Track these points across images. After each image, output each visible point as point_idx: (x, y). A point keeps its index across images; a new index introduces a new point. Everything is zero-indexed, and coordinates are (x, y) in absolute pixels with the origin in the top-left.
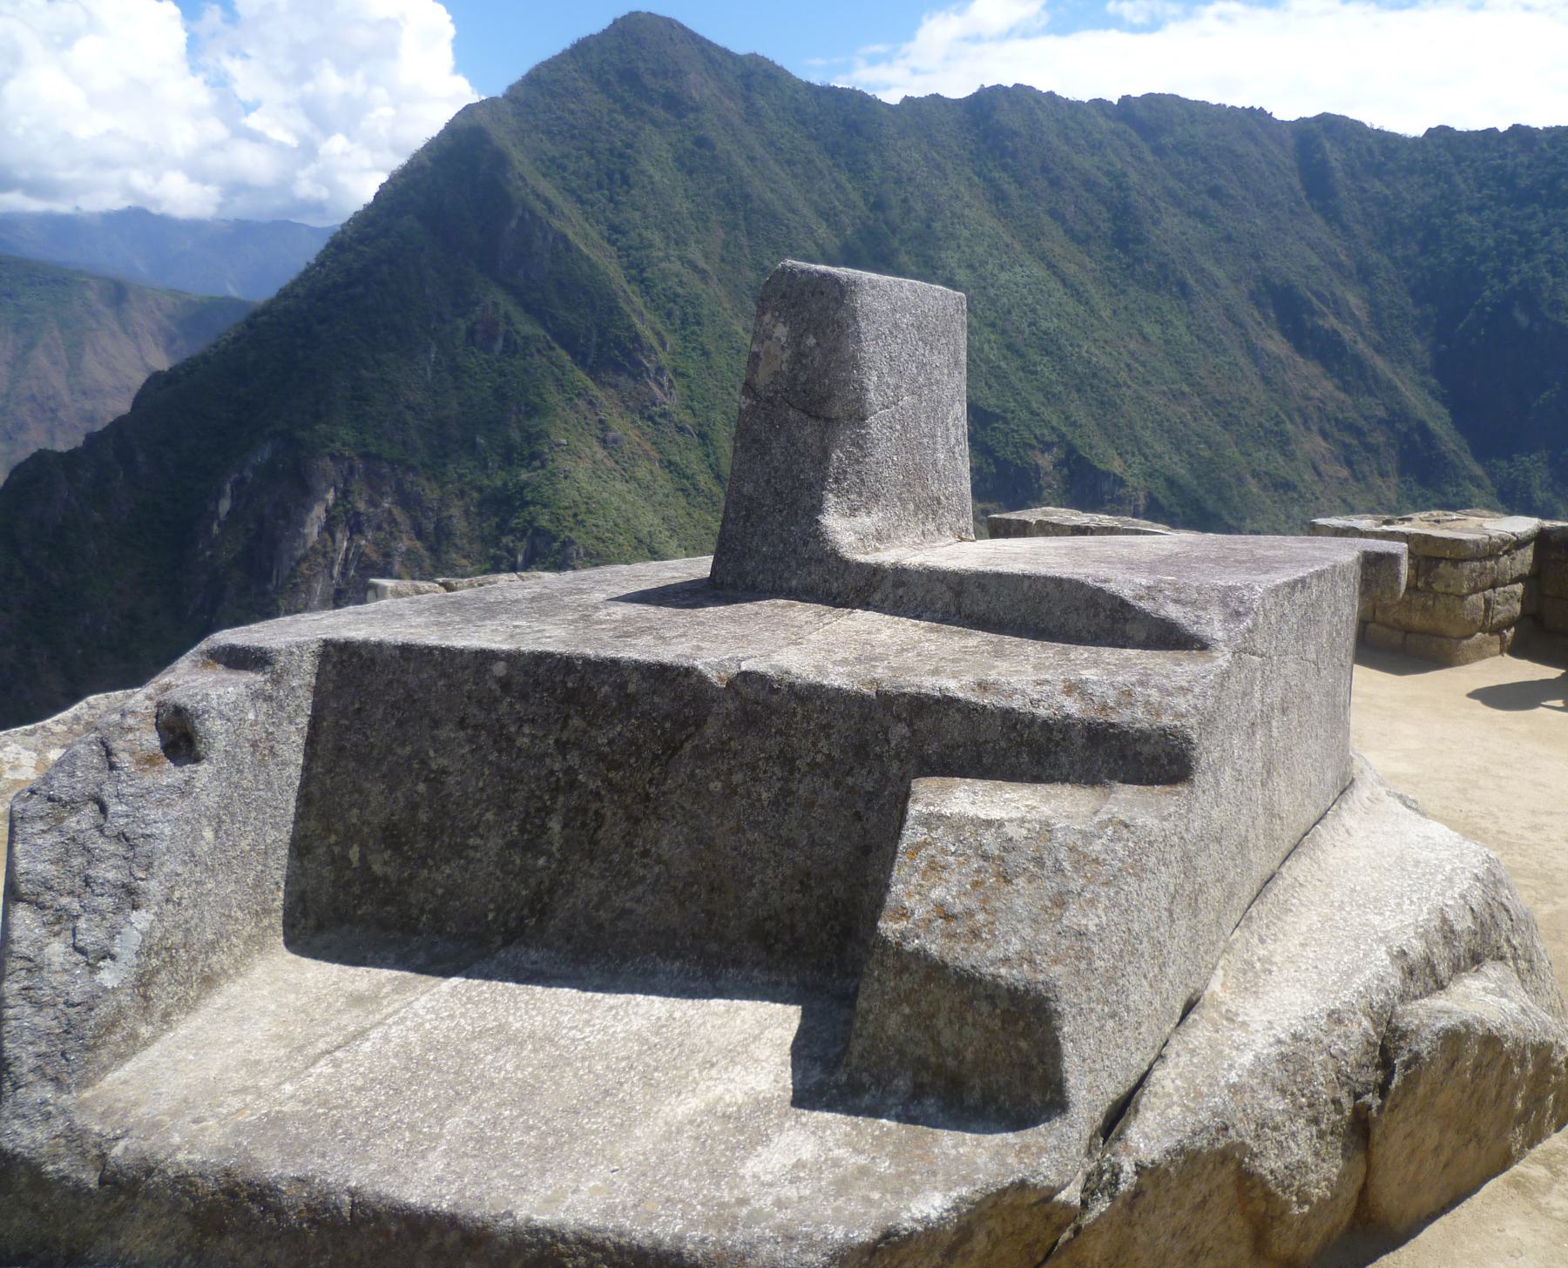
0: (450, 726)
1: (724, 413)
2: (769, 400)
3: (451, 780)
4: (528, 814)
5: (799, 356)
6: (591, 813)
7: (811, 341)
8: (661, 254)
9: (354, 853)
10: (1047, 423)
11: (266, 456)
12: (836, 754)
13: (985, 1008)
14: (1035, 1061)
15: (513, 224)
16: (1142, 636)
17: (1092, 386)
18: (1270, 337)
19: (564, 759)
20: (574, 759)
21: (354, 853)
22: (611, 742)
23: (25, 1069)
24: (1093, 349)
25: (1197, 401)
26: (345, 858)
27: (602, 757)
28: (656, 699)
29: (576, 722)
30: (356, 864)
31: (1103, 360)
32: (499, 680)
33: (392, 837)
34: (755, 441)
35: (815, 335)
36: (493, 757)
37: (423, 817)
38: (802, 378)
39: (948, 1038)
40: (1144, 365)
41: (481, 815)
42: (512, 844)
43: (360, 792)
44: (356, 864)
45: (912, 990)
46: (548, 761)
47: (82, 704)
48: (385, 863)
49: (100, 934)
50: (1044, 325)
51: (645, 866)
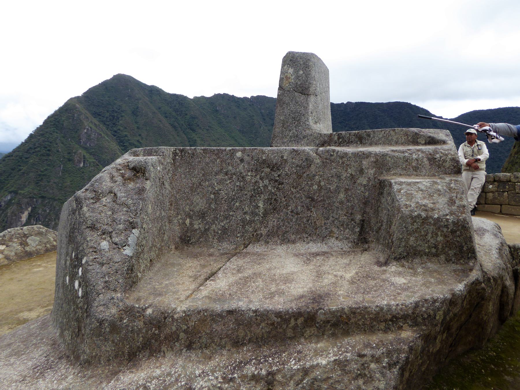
2: (288, 91)
5: (297, 77)
6: (273, 200)
9: (188, 221)
11: (9, 198)
12: (353, 173)
14: (464, 244)
16: (424, 142)
19: (263, 182)
21: (188, 221)
22: (279, 176)
23: (101, 287)
28: (294, 161)
30: (188, 224)
35: (303, 71)
36: (238, 184)
38: (299, 83)
41: (234, 204)
44: (188, 224)
45: (418, 228)
47: (6, 231)
51: (292, 216)
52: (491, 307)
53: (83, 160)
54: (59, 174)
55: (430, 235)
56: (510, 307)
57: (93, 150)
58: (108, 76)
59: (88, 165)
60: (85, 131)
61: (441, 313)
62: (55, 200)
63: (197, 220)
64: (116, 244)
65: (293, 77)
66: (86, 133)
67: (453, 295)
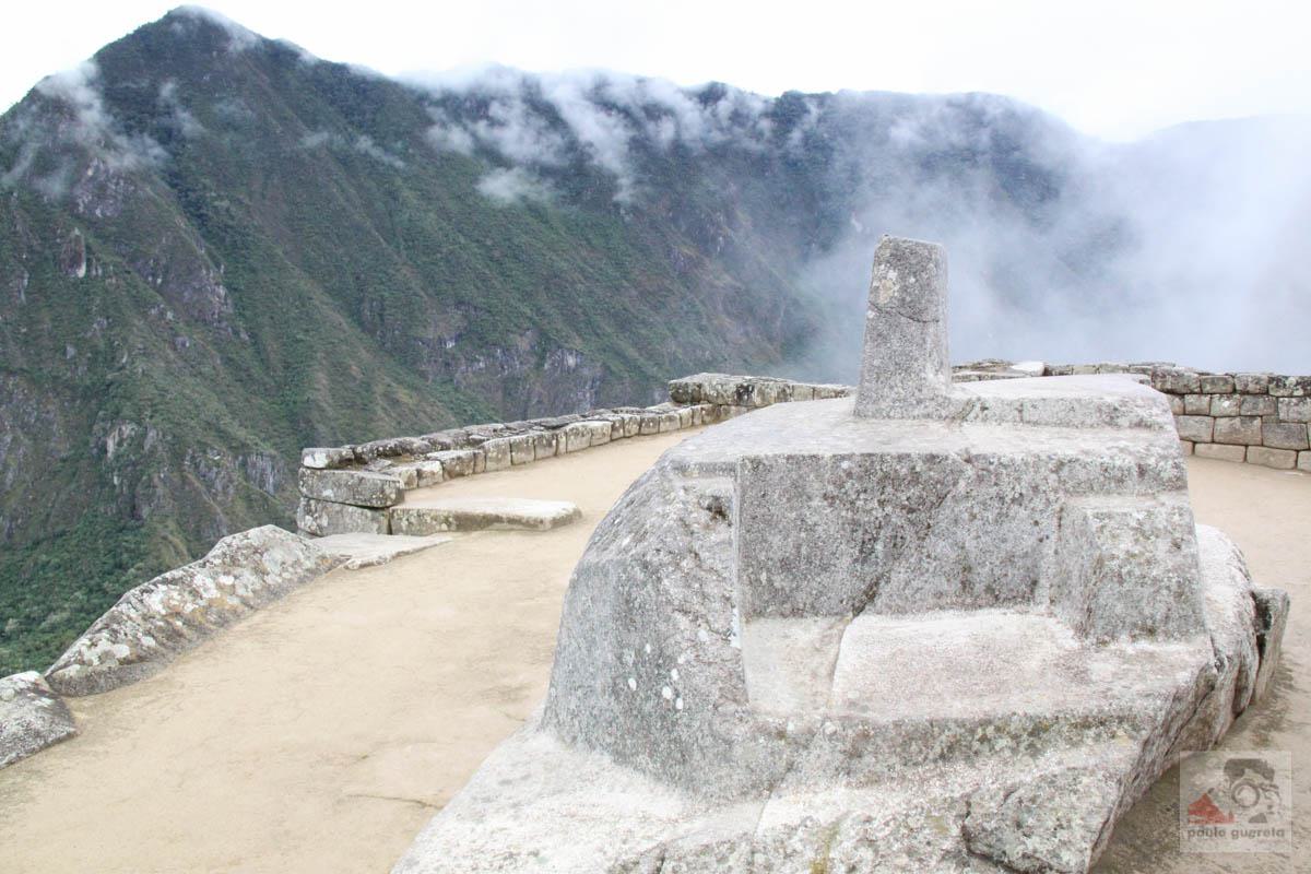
0: (818, 499)
1: (272, 318)
3: (820, 529)
4: (864, 542)
5: (904, 289)
7: (913, 280)
8: (213, 194)
9: (764, 577)
10: (523, 314)
12: (1024, 492)
13: (1165, 592)
15: (90, 173)
17: (555, 284)
18: (685, 244)
20: (889, 509)
22: (908, 499)
24: (554, 257)
25: (634, 293)
26: (758, 580)
27: (903, 507)
29: (889, 489)
30: (764, 582)
31: (564, 265)
32: (844, 471)
33: (786, 566)
34: (879, 335)
35: (915, 277)
37: (804, 551)
38: (908, 299)
39: (1147, 611)
40: (592, 267)
42: (856, 560)
43: (766, 541)
44: (764, 582)
46: (874, 512)
48: (782, 580)
49: (722, 622)
50: (516, 241)
51: (928, 563)
52: (1223, 697)
53: (84, 255)
54: (19, 298)
55: (1145, 601)
56: (1251, 692)
57: (114, 229)
58: (154, 15)
59: (100, 272)
60: (90, 173)
61: (1163, 713)
62: (12, 373)
63: (779, 574)
64: (717, 632)
65: (896, 288)
66: (92, 179)
67: (1178, 688)
